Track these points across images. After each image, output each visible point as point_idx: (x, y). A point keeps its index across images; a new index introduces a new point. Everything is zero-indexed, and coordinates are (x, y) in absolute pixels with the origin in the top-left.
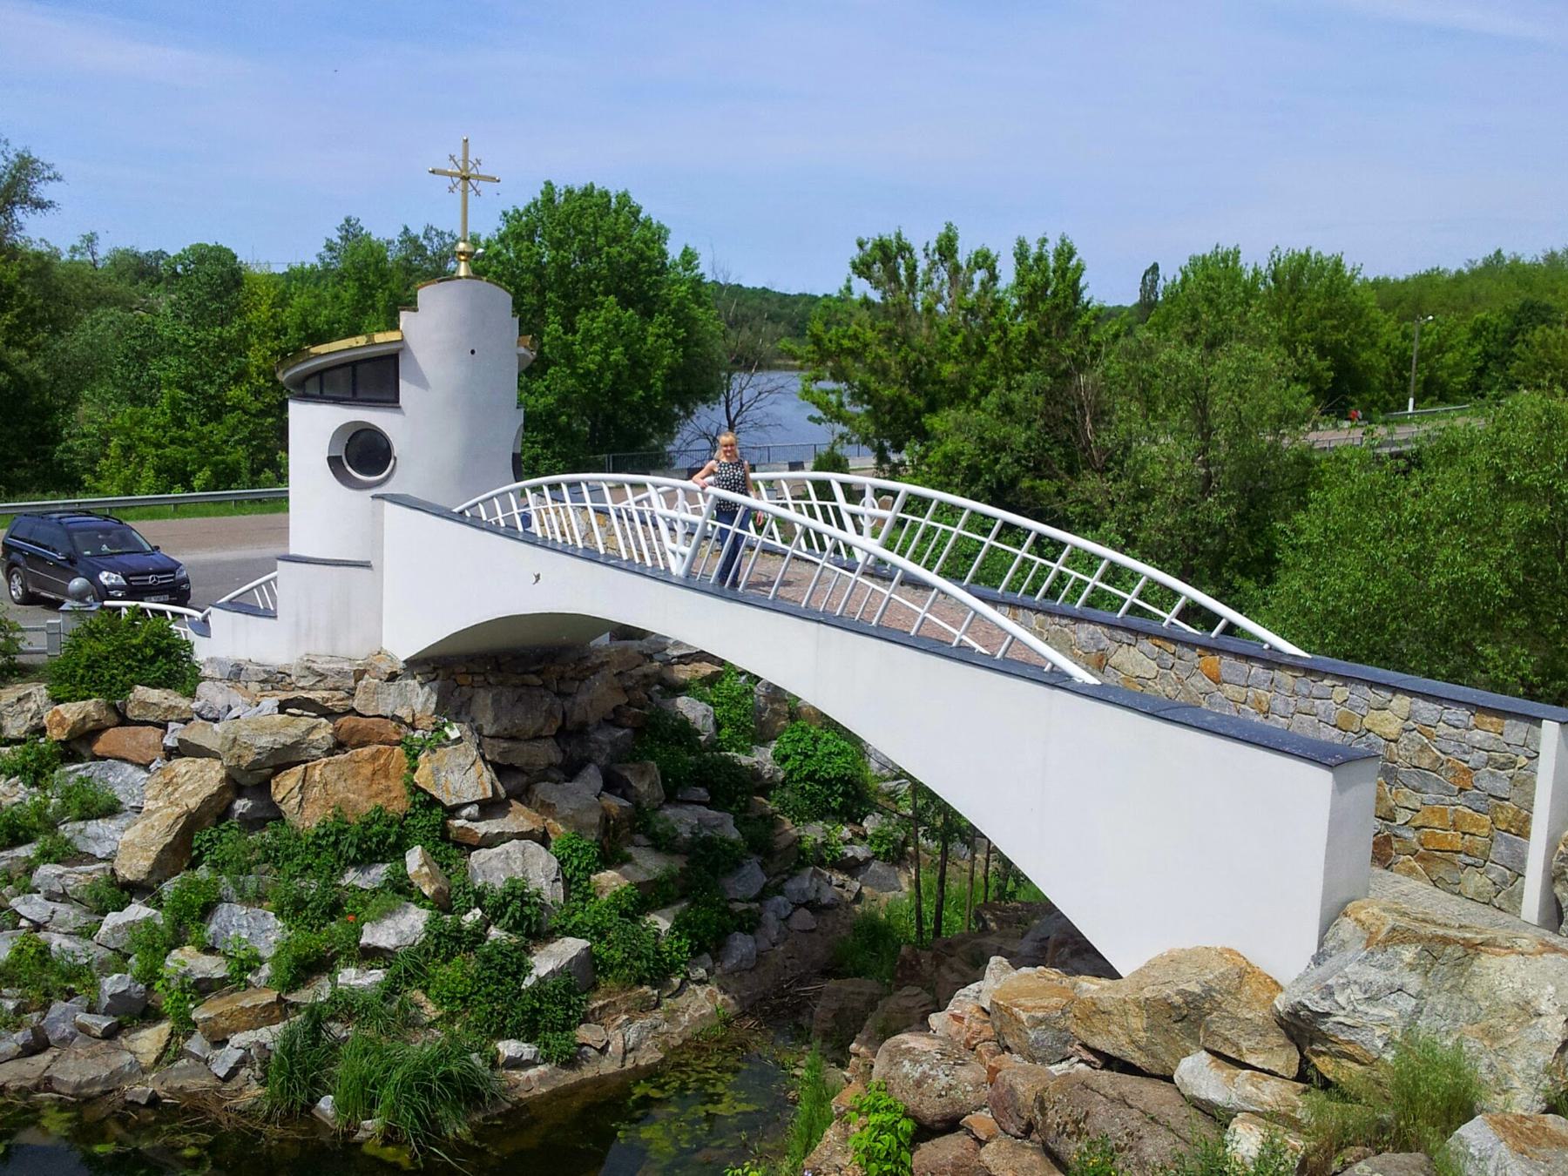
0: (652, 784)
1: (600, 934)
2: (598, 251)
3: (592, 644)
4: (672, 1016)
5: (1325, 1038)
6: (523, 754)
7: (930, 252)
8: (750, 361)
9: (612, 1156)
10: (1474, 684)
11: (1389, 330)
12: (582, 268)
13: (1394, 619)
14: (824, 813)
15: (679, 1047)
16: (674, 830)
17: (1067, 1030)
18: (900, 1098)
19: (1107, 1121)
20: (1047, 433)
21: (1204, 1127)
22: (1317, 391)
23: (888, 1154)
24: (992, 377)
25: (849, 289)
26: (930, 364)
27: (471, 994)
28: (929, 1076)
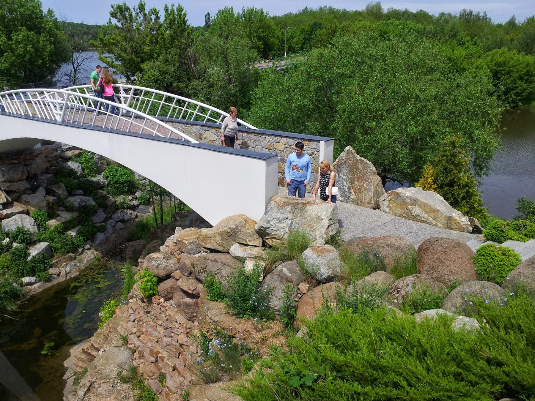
0: (63, 191)
1: (52, 240)
2: (15, 10)
3: (34, 147)
4: (80, 261)
5: (268, 234)
6: (15, 187)
7: (136, 9)
8: (81, 49)
9: (68, 305)
10: (306, 133)
11: (277, 32)
12: (10, 17)
13: (284, 117)
14: (122, 193)
15: (84, 270)
16: (73, 204)
17: (199, 244)
18: (152, 272)
19: (212, 267)
20: (180, 68)
21: (239, 264)
22: (259, 51)
23: (150, 288)
24: (161, 51)
25: (110, 22)
26: (140, 47)
27: (10, 265)
28: (160, 264)
